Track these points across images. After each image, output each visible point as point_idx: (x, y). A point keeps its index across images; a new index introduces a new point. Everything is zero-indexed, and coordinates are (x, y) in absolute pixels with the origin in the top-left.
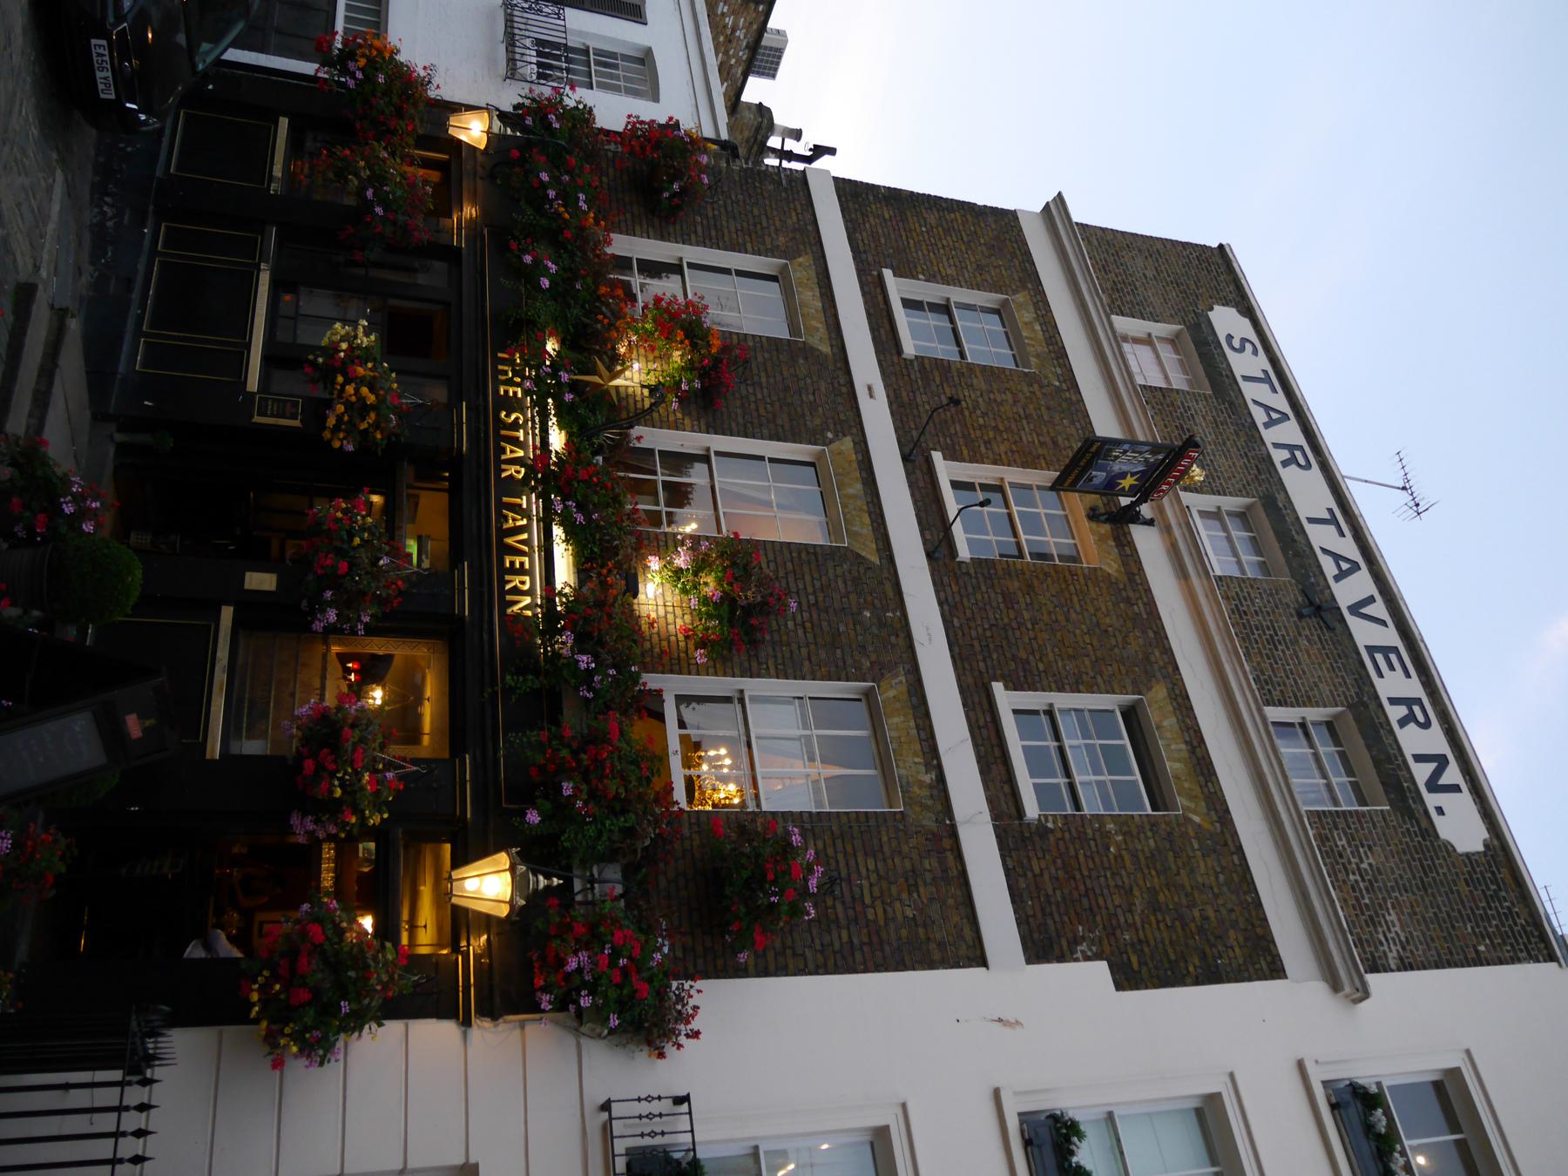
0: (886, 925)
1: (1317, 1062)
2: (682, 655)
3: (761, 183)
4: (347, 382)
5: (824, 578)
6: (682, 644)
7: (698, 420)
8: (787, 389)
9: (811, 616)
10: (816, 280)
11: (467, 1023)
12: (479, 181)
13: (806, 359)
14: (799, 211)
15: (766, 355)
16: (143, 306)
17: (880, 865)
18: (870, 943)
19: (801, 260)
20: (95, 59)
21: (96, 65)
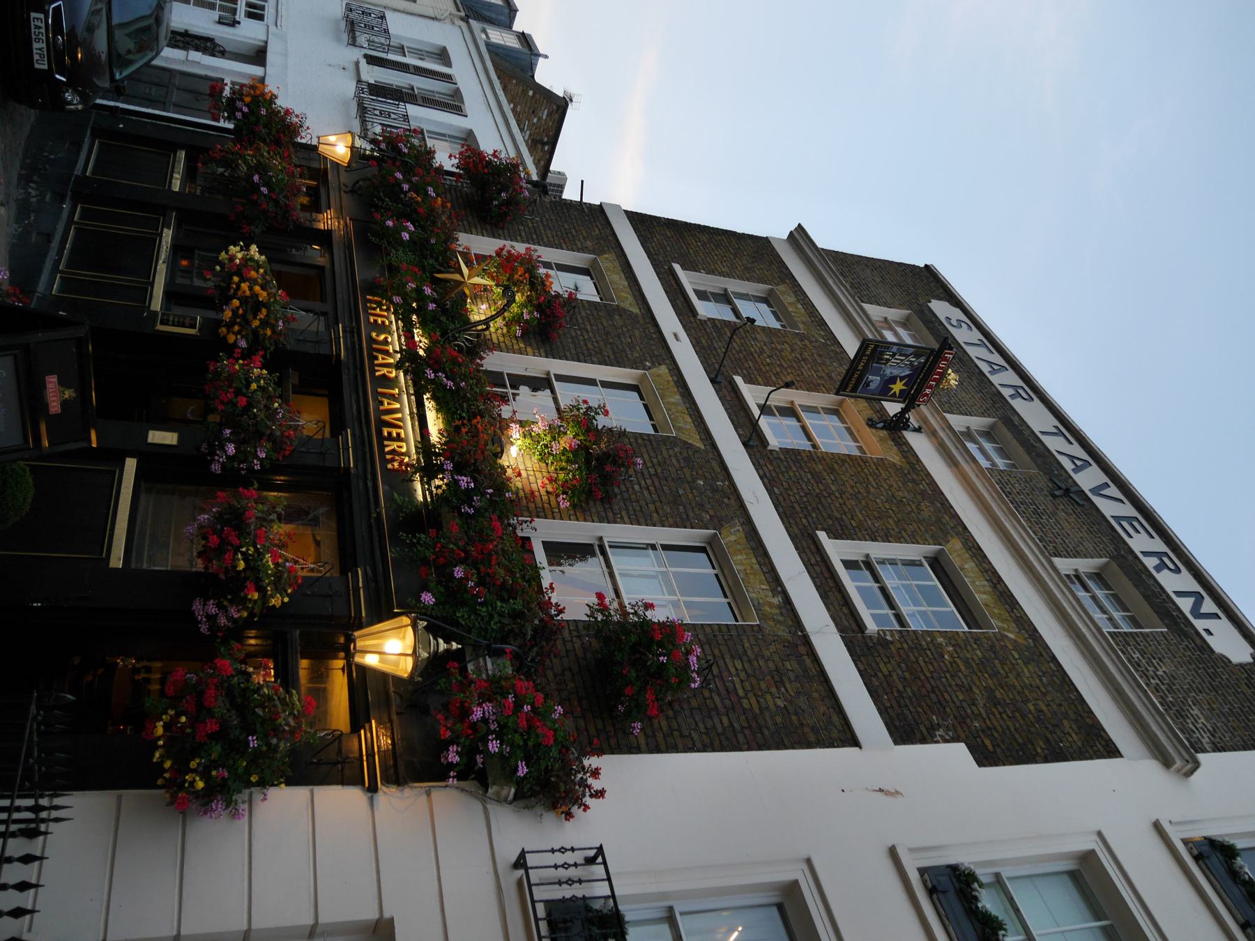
1: (1170, 822)
11: (373, 789)
20: (33, 30)
21: (34, 37)
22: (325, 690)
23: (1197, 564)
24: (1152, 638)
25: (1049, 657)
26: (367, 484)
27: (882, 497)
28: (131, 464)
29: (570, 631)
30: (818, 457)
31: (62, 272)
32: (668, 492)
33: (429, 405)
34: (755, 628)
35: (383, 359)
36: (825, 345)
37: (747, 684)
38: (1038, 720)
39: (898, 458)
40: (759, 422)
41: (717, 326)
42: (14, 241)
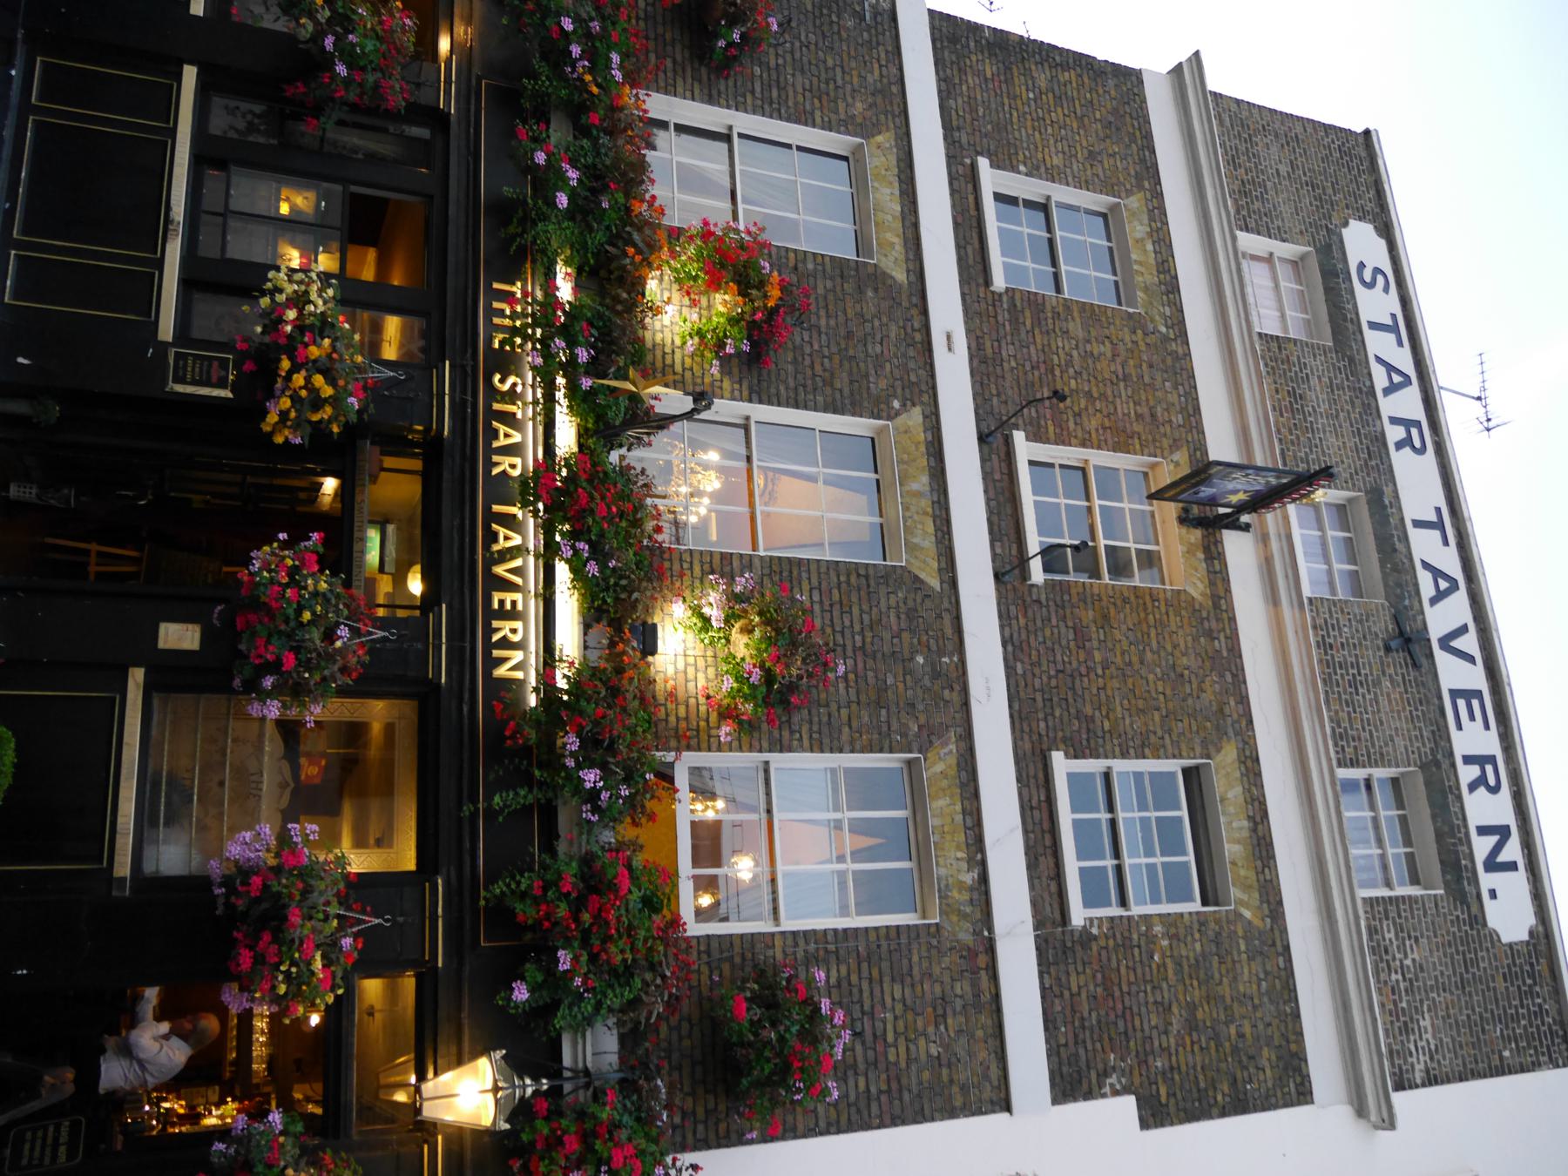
2: (702, 724)
3: (838, 17)
5: (875, 610)
6: (703, 709)
9: (856, 664)
10: (896, 171)
13: (876, 290)
14: (884, 63)
15: (829, 284)
17: (907, 991)
18: (889, 1091)
19: (879, 138)
23: (1377, 146)
24: (1420, 905)
25: (1283, 946)
26: (462, 710)
27: (1158, 670)
28: (137, 676)
29: (699, 953)
30: (1092, 595)
31: (19, 245)
32: (871, 681)
33: (562, 572)
34: (933, 930)
35: (507, 435)
36: (1165, 339)
37: (901, 1023)
38: (1235, 1050)
39: (1200, 586)
40: (1031, 562)
41: (1015, 306)
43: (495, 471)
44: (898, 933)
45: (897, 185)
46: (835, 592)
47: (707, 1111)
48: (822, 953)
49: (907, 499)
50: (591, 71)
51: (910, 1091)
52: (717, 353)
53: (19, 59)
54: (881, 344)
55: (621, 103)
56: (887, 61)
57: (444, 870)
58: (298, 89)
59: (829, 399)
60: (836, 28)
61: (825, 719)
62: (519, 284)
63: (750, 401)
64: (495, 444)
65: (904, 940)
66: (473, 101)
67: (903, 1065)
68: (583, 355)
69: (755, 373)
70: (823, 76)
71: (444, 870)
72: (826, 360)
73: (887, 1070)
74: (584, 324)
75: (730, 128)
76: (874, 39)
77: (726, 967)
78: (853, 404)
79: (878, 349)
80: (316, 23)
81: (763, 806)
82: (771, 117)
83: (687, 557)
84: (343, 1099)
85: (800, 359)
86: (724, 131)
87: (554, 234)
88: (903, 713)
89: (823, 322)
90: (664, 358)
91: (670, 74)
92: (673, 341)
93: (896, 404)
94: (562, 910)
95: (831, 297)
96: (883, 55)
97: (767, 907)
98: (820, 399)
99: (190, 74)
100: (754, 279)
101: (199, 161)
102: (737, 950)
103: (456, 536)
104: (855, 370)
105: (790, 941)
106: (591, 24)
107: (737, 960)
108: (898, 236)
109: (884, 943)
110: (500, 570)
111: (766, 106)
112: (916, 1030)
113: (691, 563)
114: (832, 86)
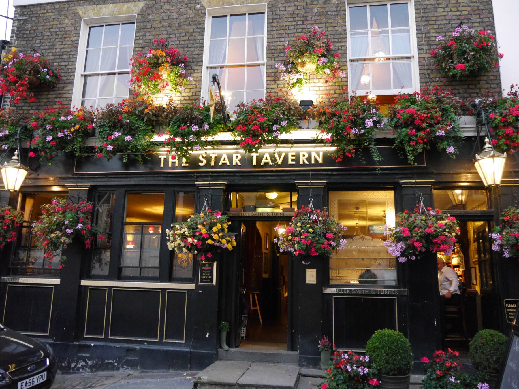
0: (470, 7)
2: (337, 84)
3: (27, 30)
4: (211, 238)
5: (287, 16)
6: (331, 84)
7: (194, 70)
8: (170, 25)
9: (310, 24)
10: (94, 6)
12: (40, 177)
13: (149, 14)
14: (46, 11)
15: (148, 34)
16: (142, 342)
17: (440, 6)
18: (479, 14)
19: (81, 13)
20: (28, 387)
21: (32, 386)
22: (368, 202)
33: (283, 136)
35: (224, 160)
37: (453, 9)
42: (139, 368)
43: (239, 164)
44: (417, 9)
45: (101, 6)
46: (280, 32)
47: (487, 84)
48: (426, 39)
49: (239, 2)
50: (69, 129)
51: (479, 6)
52: (184, 77)
53: (88, 343)
54: (172, 12)
55: (82, 116)
56: (45, 10)
57: (397, 180)
58: (88, 242)
59: (198, 34)
60: (33, 31)
61: (333, 36)
62: (160, 157)
63: (202, 65)
64: (228, 164)
65: (420, 7)
66: (82, 176)
67: (469, 8)
68: (195, 128)
69: (190, 64)
70: (54, 36)
71: (397, 180)
72: (181, 35)
73: (471, 15)
74: (180, 129)
75: (82, 75)
76: (35, 15)
77: (432, 76)
78: (200, 24)
79: (174, 14)
80: (62, 236)
81: (362, 62)
82: (76, 58)
83: (269, 90)
84: (480, 214)
85: (182, 46)
86: (83, 78)
87: (143, 141)
88: (329, 5)
89: (165, 36)
90: (186, 100)
91: (62, 99)
92: (179, 96)
93: (198, 6)
94: (421, 134)
95: (153, 33)
96: (43, 11)
97: (405, 61)
98: (198, 38)
99: (84, 283)
100: (155, 60)
101: (120, 278)
102: (425, 71)
103: (266, 178)
104: (185, 23)
105: (422, 51)
106: (48, 129)
107: (429, 71)
108: (124, 5)
109: (422, 15)
110: (280, 162)
111: (71, 60)
112: (456, 3)
113: (271, 88)
114: (59, 33)
